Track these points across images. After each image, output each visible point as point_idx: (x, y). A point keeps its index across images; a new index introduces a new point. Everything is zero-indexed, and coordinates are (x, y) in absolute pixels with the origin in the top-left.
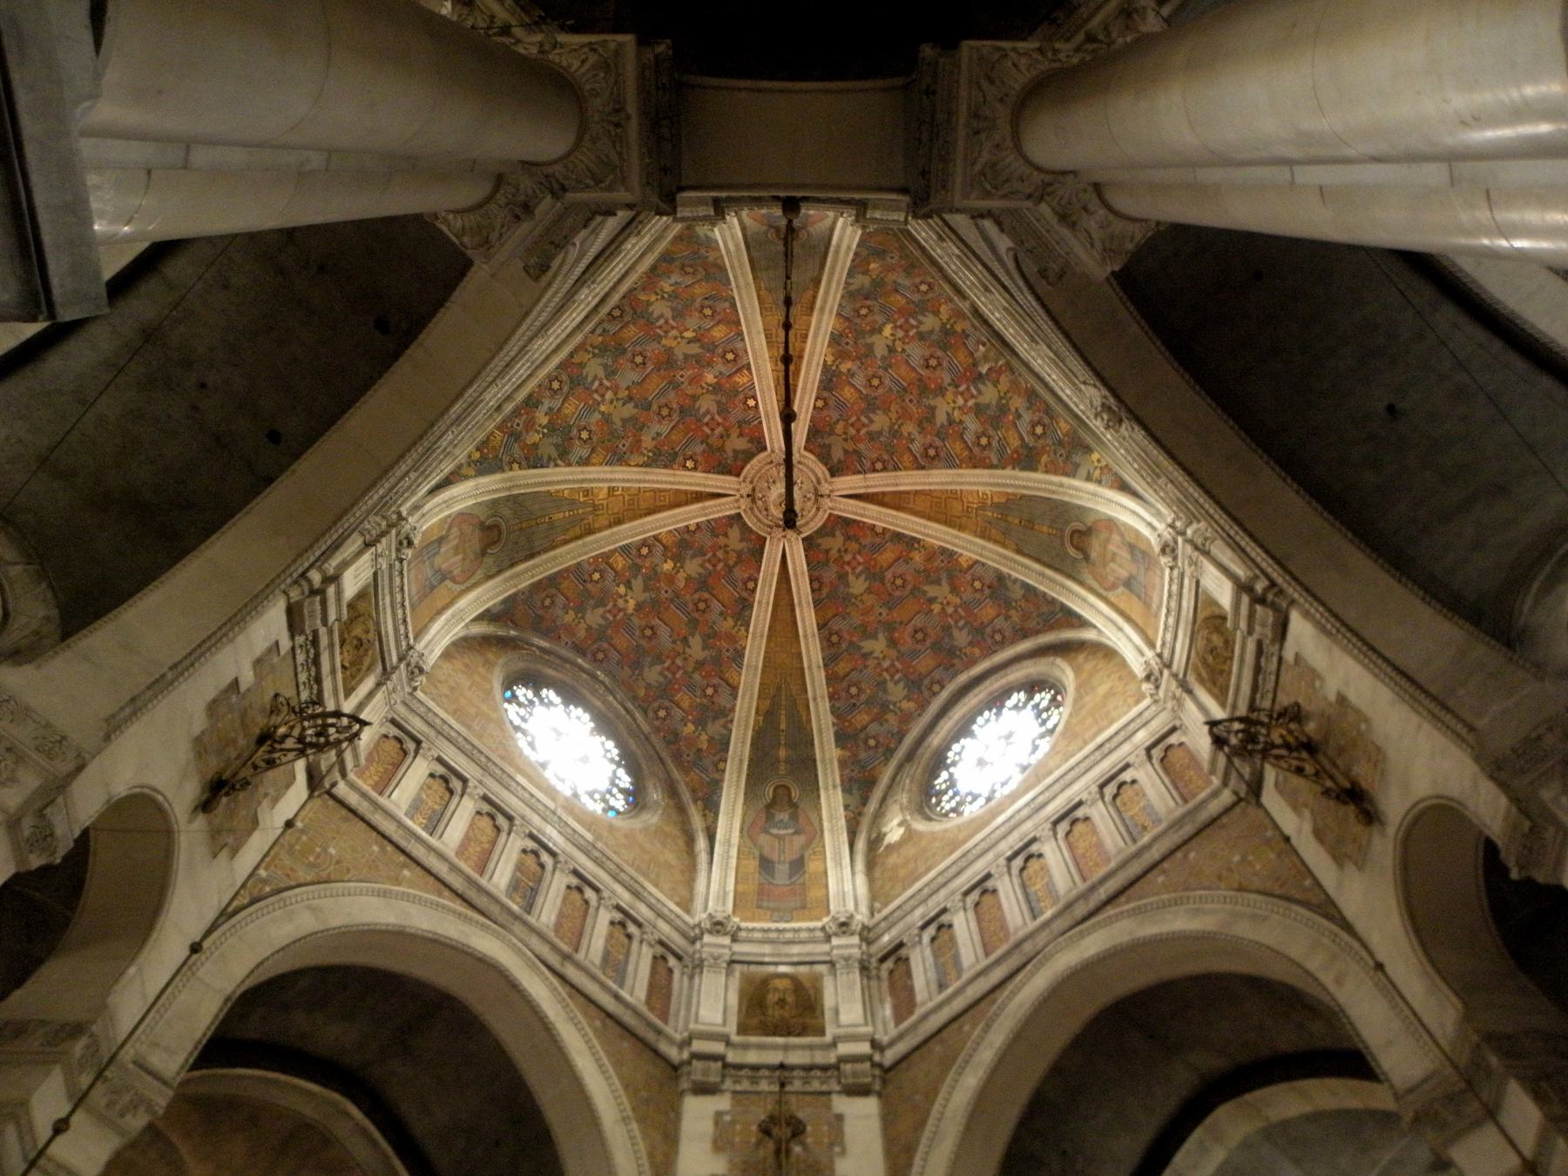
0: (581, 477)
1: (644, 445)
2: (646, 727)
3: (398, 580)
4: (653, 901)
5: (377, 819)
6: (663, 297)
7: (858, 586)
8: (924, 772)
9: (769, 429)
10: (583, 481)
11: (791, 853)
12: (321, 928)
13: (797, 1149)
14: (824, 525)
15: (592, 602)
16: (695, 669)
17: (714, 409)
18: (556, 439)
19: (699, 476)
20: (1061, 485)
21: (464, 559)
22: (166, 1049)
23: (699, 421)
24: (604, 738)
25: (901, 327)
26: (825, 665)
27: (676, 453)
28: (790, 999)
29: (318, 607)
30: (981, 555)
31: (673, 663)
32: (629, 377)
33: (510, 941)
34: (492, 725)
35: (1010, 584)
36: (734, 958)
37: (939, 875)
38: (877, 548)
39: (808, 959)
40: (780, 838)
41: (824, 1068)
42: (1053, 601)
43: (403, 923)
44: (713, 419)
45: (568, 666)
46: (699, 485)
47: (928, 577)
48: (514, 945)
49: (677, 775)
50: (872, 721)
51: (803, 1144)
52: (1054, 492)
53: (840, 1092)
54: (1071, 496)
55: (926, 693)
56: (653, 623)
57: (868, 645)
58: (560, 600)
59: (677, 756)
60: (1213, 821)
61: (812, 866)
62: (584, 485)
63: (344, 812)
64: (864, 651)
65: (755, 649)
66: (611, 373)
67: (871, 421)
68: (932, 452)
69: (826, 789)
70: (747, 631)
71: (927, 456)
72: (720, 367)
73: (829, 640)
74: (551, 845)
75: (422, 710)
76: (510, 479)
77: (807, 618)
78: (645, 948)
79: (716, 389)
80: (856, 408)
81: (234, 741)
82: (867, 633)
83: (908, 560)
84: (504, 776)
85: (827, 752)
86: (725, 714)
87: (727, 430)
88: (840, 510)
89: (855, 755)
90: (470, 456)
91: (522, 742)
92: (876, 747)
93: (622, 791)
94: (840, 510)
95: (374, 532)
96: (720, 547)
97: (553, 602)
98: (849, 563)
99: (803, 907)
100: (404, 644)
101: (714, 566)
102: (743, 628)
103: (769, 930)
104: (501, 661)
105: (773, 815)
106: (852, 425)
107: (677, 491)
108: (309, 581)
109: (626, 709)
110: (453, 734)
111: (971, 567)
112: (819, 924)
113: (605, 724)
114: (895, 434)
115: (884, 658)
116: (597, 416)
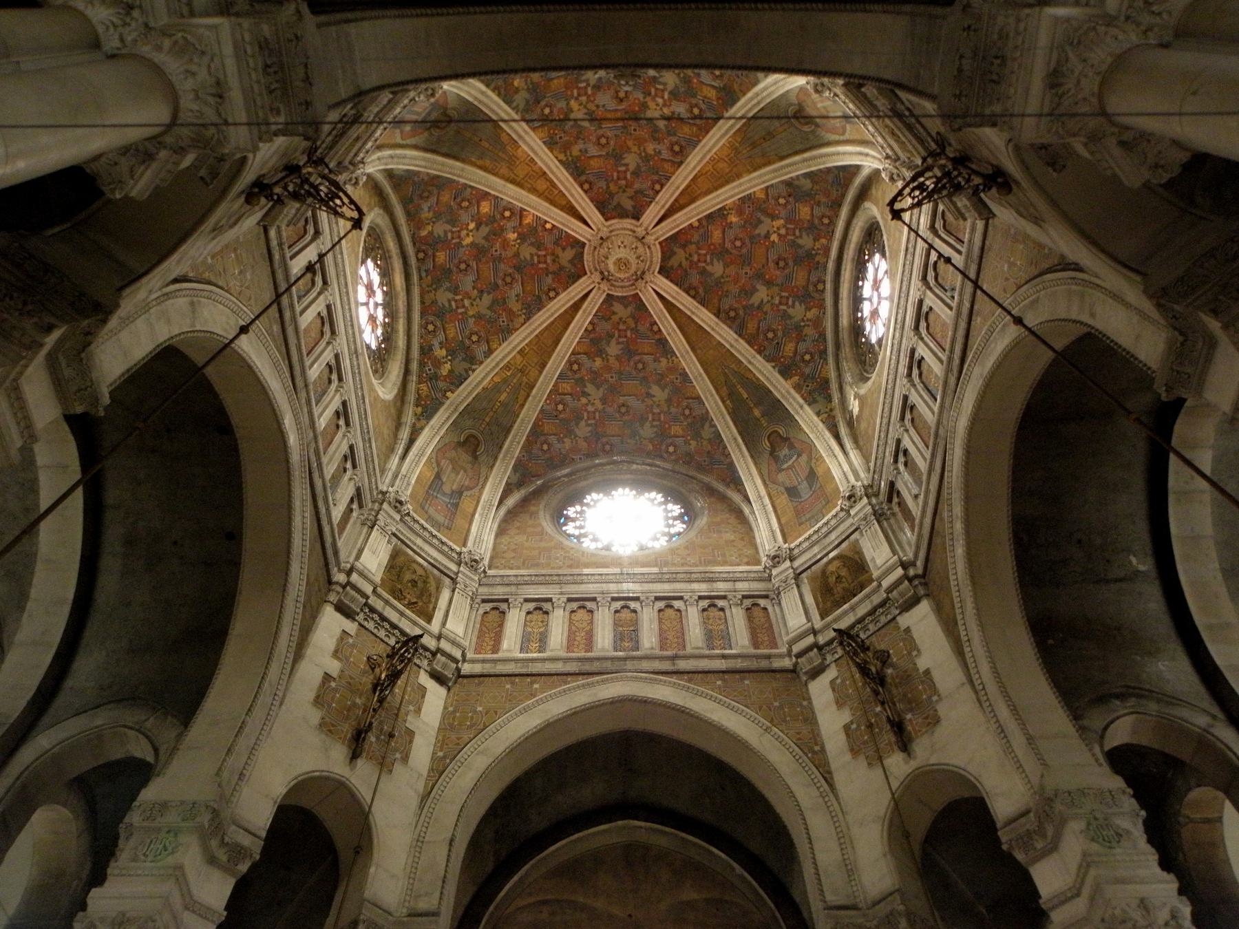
1: (515, 309)
2: (668, 466)
5: (501, 668)
6: (434, 222)
7: (717, 269)
9: (573, 230)
10: (497, 364)
11: (803, 474)
12: (492, 760)
13: (890, 671)
14: (663, 252)
16: (669, 407)
17: (534, 250)
19: (563, 296)
20: (757, 94)
21: (465, 471)
22: (427, 894)
23: (532, 265)
24: (646, 494)
25: (579, 95)
26: (740, 336)
28: (844, 572)
29: (353, 593)
30: (764, 182)
31: (654, 414)
32: (467, 282)
33: (627, 677)
35: (796, 183)
36: (798, 572)
38: (706, 236)
40: (792, 467)
41: (882, 604)
42: (829, 170)
44: (539, 256)
47: (751, 224)
49: (706, 479)
51: (893, 665)
52: (759, 103)
54: (768, 95)
55: (816, 295)
57: (755, 300)
58: (552, 439)
59: (700, 468)
60: (982, 249)
61: (820, 471)
63: (476, 680)
65: (691, 364)
66: (456, 290)
67: (627, 165)
68: (677, 148)
69: (798, 413)
71: (677, 153)
72: (510, 225)
73: (729, 318)
76: (451, 404)
77: (704, 317)
79: (522, 237)
80: (609, 167)
81: (354, 705)
82: (748, 292)
83: (730, 225)
85: (783, 389)
86: (705, 418)
87: (553, 254)
88: (662, 235)
89: (802, 375)
90: (416, 414)
91: (587, 544)
92: (812, 357)
93: (675, 519)
94: (662, 235)
95: (371, 517)
96: (618, 323)
97: (549, 444)
99: (828, 502)
103: (810, 536)
104: (541, 506)
106: (619, 179)
108: (337, 583)
109: (649, 465)
110: (526, 578)
111: (767, 194)
113: (642, 484)
114: (646, 158)
115: (772, 298)
116: (471, 321)
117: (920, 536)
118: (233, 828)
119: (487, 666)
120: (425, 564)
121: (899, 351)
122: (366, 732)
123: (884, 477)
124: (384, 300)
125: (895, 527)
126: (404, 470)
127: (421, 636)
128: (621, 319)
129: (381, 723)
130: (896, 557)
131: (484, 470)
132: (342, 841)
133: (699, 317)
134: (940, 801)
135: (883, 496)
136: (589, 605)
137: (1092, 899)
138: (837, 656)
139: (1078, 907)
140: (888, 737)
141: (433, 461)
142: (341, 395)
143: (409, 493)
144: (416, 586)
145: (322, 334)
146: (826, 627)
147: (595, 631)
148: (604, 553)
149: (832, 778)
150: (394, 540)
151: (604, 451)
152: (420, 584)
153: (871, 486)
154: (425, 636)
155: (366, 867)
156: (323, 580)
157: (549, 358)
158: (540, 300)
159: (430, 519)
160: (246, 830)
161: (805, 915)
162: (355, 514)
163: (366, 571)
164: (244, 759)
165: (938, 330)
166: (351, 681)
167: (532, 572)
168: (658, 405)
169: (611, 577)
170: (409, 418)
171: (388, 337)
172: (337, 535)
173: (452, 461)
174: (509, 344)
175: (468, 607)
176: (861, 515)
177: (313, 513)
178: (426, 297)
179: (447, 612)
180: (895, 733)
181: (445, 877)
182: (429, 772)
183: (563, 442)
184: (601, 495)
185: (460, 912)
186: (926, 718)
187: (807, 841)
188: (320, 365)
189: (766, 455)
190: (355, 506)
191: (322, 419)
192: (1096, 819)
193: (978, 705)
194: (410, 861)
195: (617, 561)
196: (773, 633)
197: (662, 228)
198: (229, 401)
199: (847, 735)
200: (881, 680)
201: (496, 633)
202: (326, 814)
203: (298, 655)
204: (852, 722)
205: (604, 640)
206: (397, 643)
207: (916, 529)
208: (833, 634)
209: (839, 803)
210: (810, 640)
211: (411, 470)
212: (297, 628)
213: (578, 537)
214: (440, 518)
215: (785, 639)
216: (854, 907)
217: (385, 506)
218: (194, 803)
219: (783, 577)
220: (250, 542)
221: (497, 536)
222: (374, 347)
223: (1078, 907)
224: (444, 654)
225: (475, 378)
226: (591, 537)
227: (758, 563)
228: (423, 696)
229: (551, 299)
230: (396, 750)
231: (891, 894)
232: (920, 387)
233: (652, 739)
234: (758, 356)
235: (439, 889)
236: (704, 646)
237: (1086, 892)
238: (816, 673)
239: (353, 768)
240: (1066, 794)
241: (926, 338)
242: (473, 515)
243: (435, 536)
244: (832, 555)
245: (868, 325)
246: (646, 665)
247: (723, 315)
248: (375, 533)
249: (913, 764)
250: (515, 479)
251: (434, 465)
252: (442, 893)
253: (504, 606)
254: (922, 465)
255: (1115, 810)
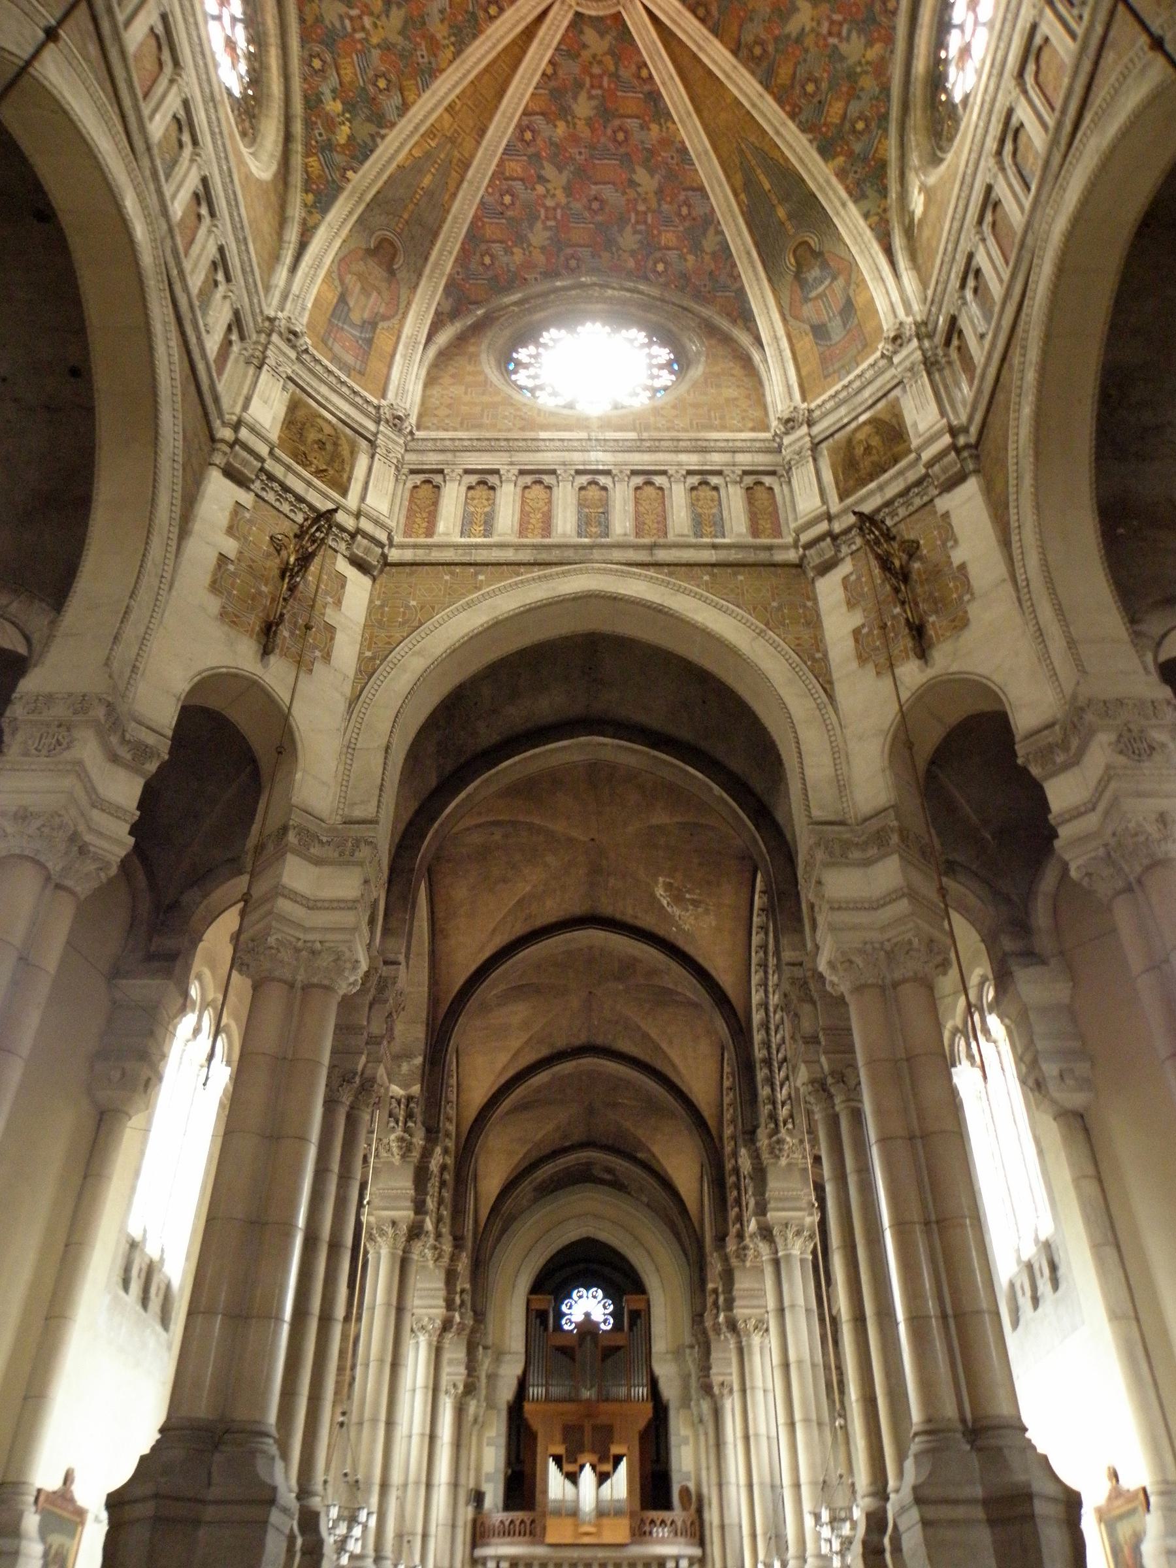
0: (410, 128)
1: (439, 36)
2: (655, 292)
3: (318, 368)
4: (722, 444)
5: (436, 556)
8: (924, 110)
10: (416, 128)
11: (837, 302)
12: (430, 661)
13: (917, 565)
15: (525, 224)
16: (659, 201)
18: (363, 113)
22: (362, 802)
26: (767, 88)
27: (473, 14)
28: (875, 441)
29: (244, 454)
33: (593, 569)
34: (500, 408)
36: (817, 440)
37: (952, 222)
39: (880, 394)
41: (919, 483)
43: (494, 615)
45: (552, 296)
46: (518, 22)
48: (599, 569)
49: (706, 312)
50: (848, 103)
51: (921, 559)
53: (940, 494)
55: (884, 20)
56: (593, 193)
58: (497, 248)
59: (698, 296)
61: (859, 301)
62: (422, 130)
63: (407, 569)
64: (794, 35)
70: (674, 123)
74: (601, 467)
75: (430, 444)
78: (731, 489)
81: (260, 593)
84: (529, 443)
86: (709, 221)
89: (850, 154)
90: (306, 205)
91: (545, 400)
95: (257, 353)
99: (865, 346)
100: (370, 409)
101: (601, 87)
102: (669, 124)
103: (837, 393)
104: (484, 346)
105: (806, 279)
107: (505, 49)
108: (222, 441)
109: (628, 290)
110: (466, 443)
112: (878, 354)
113: (620, 316)
116: (376, 53)
117: (979, 391)
118: (133, 724)
119: (420, 552)
120: (334, 420)
121: (991, 112)
122: (278, 625)
123: (944, 310)
124: (244, 13)
125: (949, 381)
126: (295, 289)
127: (335, 510)
128: (594, 56)
129: (294, 615)
130: (945, 421)
131: (404, 292)
132: (260, 743)
133: (709, 56)
134: (954, 716)
135: (939, 338)
136: (547, 479)
137: (1107, 813)
138: (854, 547)
139: (1092, 821)
140: (905, 642)
141: (335, 276)
142: (199, 167)
143: (305, 320)
144: (325, 449)
145: (161, 65)
146: (844, 511)
147: (554, 512)
148: (566, 412)
149: (833, 689)
150: (291, 385)
151: (567, 267)
152: (329, 447)
153: (925, 323)
154: (340, 511)
155: (291, 773)
156: (203, 437)
157: (490, 119)
158: (476, 21)
159: (335, 359)
160: (148, 728)
161: (789, 837)
162: (235, 348)
163: (258, 426)
164: (135, 650)
165: (1051, 76)
166: (254, 565)
167: (473, 434)
168: (645, 200)
169: (575, 444)
170: (296, 211)
171: (256, 78)
172: (215, 374)
173: (360, 276)
174: (433, 94)
175: (392, 479)
176: (907, 364)
177: (181, 343)
178: (307, 9)
179: (367, 483)
180: (913, 638)
181: (382, 785)
182: (356, 674)
183: (512, 253)
184: (563, 332)
185: (402, 827)
186: (953, 621)
187: (796, 755)
188: (164, 116)
189: (789, 277)
190: (234, 337)
191: (176, 204)
192: (1130, 730)
193: (1017, 604)
194: (341, 768)
195: (582, 423)
196: (778, 518)
198: (45, 168)
199: (856, 641)
200: (905, 576)
201: (430, 513)
202: (239, 717)
203: (184, 533)
204: (863, 626)
205: (565, 524)
206: (306, 520)
207: (976, 382)
208: (852, 519)
209: (839, 718)
210: (823, 527)
211: (305, 289)
212: (178, 495)
213: (532, 391)
214: (349, 359)
215: (793, 525)
216: (842, 823)
217: (275, 338)
218: (84, 696)
219: (796, 447)
220: (103, 380)
221: (426, 385)
222: (237, 93)
223: (1092, 821)
224: (365, 535)
225: (387, 148)
226: (549, 390)
227: (766, 428)
228: (343, 586)
229: (492, 18)
230: (316, 647)
231: (885, 810)
232: (1011, 171)
233: (622, 644)
234: (790, 123)
235: (376, 799)
236: (691, 533)
237: (1101, 807)
238: (826, 568)
239: (266, 666)
240: (1102, 704)
241: (1031, 93)
242: (393, 356)
243: (343, 383)
244: (862, 418)
245: (952, 71)
246: (617, 555)
247: (744, 52)
248: (264, 376)
249: (931, 672)
250: (447, 307)
251: (337, 283)
252: (379, 801)
253: (438, 479)
254: (996, 289)
255: (1154, 721)
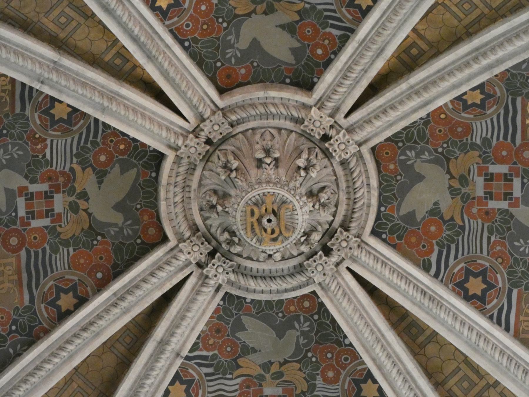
98: (48, 196)
197: (169, 278)
